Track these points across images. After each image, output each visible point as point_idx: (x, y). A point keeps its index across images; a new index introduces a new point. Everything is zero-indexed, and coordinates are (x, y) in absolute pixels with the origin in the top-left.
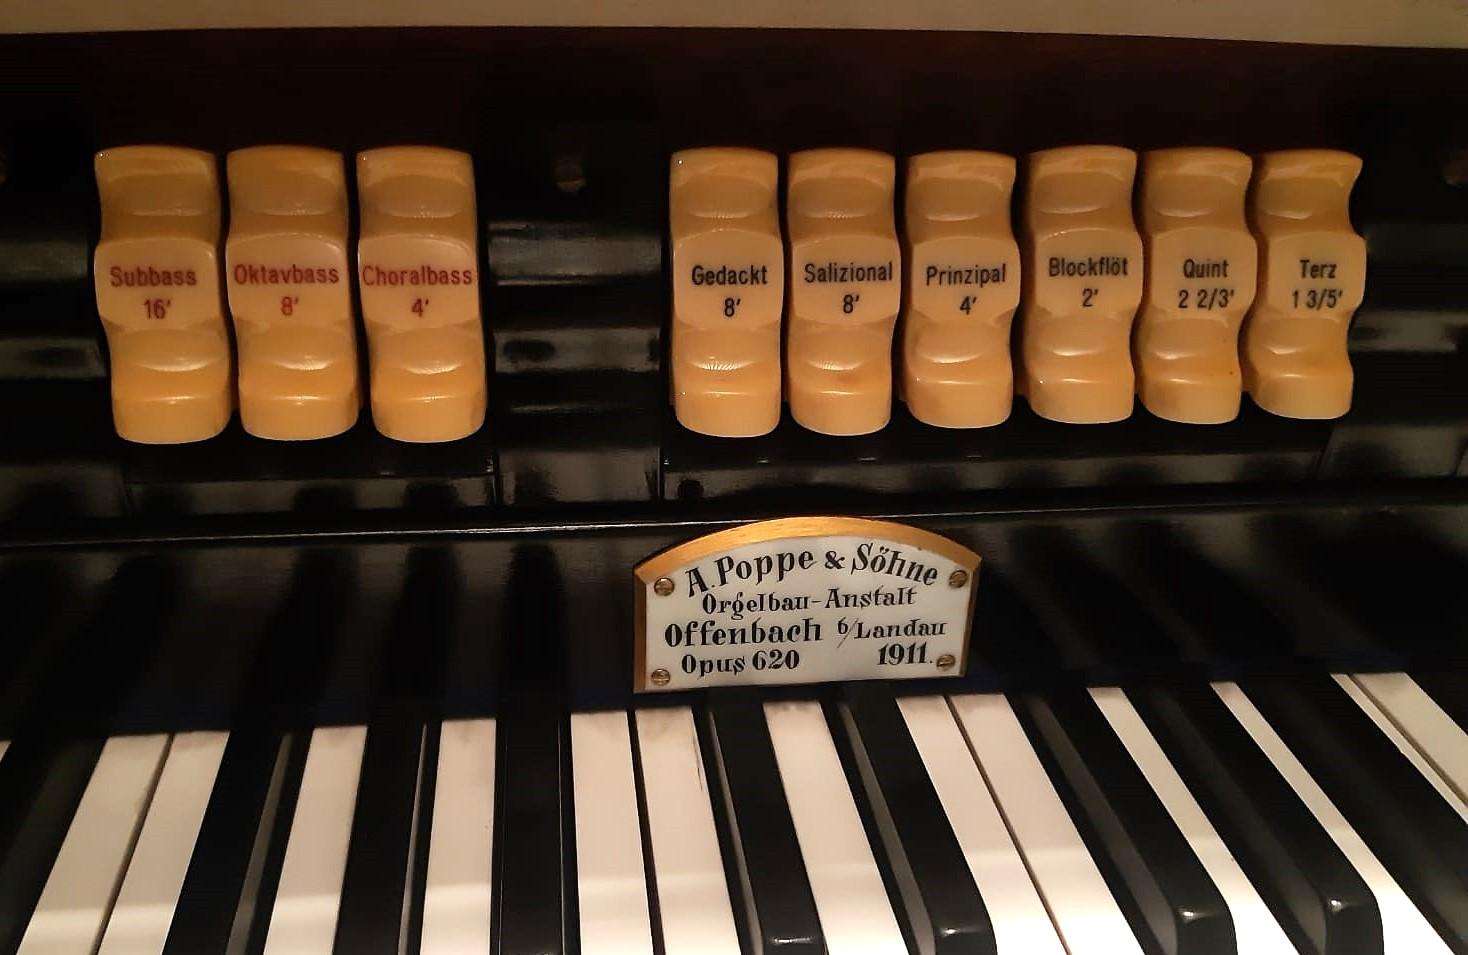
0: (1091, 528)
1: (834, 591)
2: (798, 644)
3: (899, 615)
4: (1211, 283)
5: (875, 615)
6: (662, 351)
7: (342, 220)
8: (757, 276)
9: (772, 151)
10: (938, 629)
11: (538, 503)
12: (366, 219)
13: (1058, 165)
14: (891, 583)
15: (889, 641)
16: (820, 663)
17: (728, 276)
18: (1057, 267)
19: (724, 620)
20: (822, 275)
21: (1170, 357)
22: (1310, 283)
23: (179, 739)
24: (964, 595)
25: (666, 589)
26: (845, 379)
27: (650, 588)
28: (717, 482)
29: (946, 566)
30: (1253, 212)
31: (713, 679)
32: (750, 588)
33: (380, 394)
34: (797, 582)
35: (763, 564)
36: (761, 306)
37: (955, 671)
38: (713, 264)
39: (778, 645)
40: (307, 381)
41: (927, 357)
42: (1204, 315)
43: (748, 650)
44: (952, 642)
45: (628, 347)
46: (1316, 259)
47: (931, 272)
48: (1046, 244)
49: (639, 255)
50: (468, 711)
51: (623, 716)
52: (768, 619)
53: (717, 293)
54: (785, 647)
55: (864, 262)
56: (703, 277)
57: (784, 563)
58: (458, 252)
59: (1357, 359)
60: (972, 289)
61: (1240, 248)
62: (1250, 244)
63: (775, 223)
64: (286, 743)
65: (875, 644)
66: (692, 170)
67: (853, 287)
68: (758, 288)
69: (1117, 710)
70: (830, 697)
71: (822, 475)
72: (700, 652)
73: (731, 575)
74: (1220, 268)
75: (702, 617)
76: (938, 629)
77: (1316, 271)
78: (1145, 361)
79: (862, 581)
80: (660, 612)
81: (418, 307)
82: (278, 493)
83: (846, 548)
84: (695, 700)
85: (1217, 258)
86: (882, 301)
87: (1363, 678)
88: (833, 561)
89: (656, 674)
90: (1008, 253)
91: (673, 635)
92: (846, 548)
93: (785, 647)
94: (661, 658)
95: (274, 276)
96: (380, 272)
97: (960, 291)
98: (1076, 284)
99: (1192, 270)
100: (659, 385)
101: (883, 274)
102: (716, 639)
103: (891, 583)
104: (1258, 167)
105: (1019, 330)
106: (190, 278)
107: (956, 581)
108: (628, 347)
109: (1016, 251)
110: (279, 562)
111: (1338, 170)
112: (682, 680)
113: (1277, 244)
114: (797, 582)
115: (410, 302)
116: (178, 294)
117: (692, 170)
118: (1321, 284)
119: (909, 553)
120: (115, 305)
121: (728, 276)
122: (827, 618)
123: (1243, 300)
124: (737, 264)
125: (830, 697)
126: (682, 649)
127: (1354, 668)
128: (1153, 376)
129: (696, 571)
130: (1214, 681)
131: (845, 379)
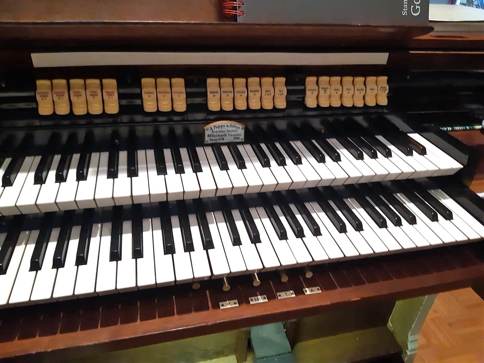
0: (331, 119)
1: (228, 130)
2: (224, 137)
3: (236, 133)
4: (268, 93)
5: (233, 133)
6: (207, 100)
7: (84, 87)
8: (217, 92)
9: (168, 78)
10: (241, 135)
11: (132, 121)
12: (87, 87)
13: (250, 80)
14: (234, 129)
15: (235, 137)
16: (227, 139)
17: (214, 92)
18: (251, 91)
19: (215, 134)
20: (224, 92)
21: (265, 101)
22: (280, 92)
23: (36, 157)
24: (243, 131)
25: (208, 130)
26: (228, 104)
27: (206, 130)
28: (212, 117)
29: (241, 127)
30: (85, 87)
31: (214, 142)
32: (218, 130)
33: (174, 106)
34: (223, 129)
35: (219, 127)
36: (218, 96)
37: (243, 141)
38: (212, 91)
39: (221, 137)
40: (165, 105)
41: (109, 104)
42: (268, 97)
43: (217, 138)
44: (242, 137)
45: (138, 102)
46: (280, 90)
47: (237, 92)
48: (249, 89)
49: (204, 90)
50: (123, 150)
51: (144, 151)
52: (220, 134)
53: (213, 95)
54: (222, 137)
55: (229, 91)
56: (211, 92)
57: (222, 126)
58: (184, 90)
59: (287, 102)
60: (241, 94)
61: (83, 92)
62: (353, 87)
63: (219, 87)
64: (69, 157)
65: (233, 137)
66: (144, 81)
67: (228, 94)
68: (315, 91)
69: (314, 141)
70: (228, 144)
71: (225, 116)
72: (212, 138)
73: (215, 128)
74: (269, 91)
75: (212, 133)
76: (241, 135)
77: (281, 91)
78: (342, 100)
79: (230, 129)
80: (207, 133)
81: (164, 96)
82: (110, 120)
83: (229, 125)
84: (211, 145)
85: (269, 90)
86: (231, 95)
87: (330, 139)
88: (228, 126)
89: (206, 141)
90: (364, 88)
91: (208, 136)
92: (229, 125)
93: (222, 137)
94: (207, 139)
95: (163, 93)
96: (175, 92)
97: (240, 94)
98: (148, 95)
99: (266, 91)
100: (206, 105)
101: (231, 92)
102: (214, 136)
103: (234, 129)
104: (85, 82)
105: (341, 96)
106: (315, 90)
107: (242, 129)
108: (138, 102)
109: (365, 87)
110: (109, 130)
111: (283, 80)
112: (210, 142)
113: (344, 87)
114: (223, 129)
115: (359, 92)
116: (216, 94)
117: (144, 81)
118: (282, 92)
119: (237, 125)
120: (38, 98)
121: (214, 92)
122: (227, 133)
123: (272, 95)
124: (215, 91)
125: (228, 144)
126: (210, 138)
127: (328, 138)
128: (378, 100)
129: (211, 128)
130: (290, 141)
131: (228, 104)
